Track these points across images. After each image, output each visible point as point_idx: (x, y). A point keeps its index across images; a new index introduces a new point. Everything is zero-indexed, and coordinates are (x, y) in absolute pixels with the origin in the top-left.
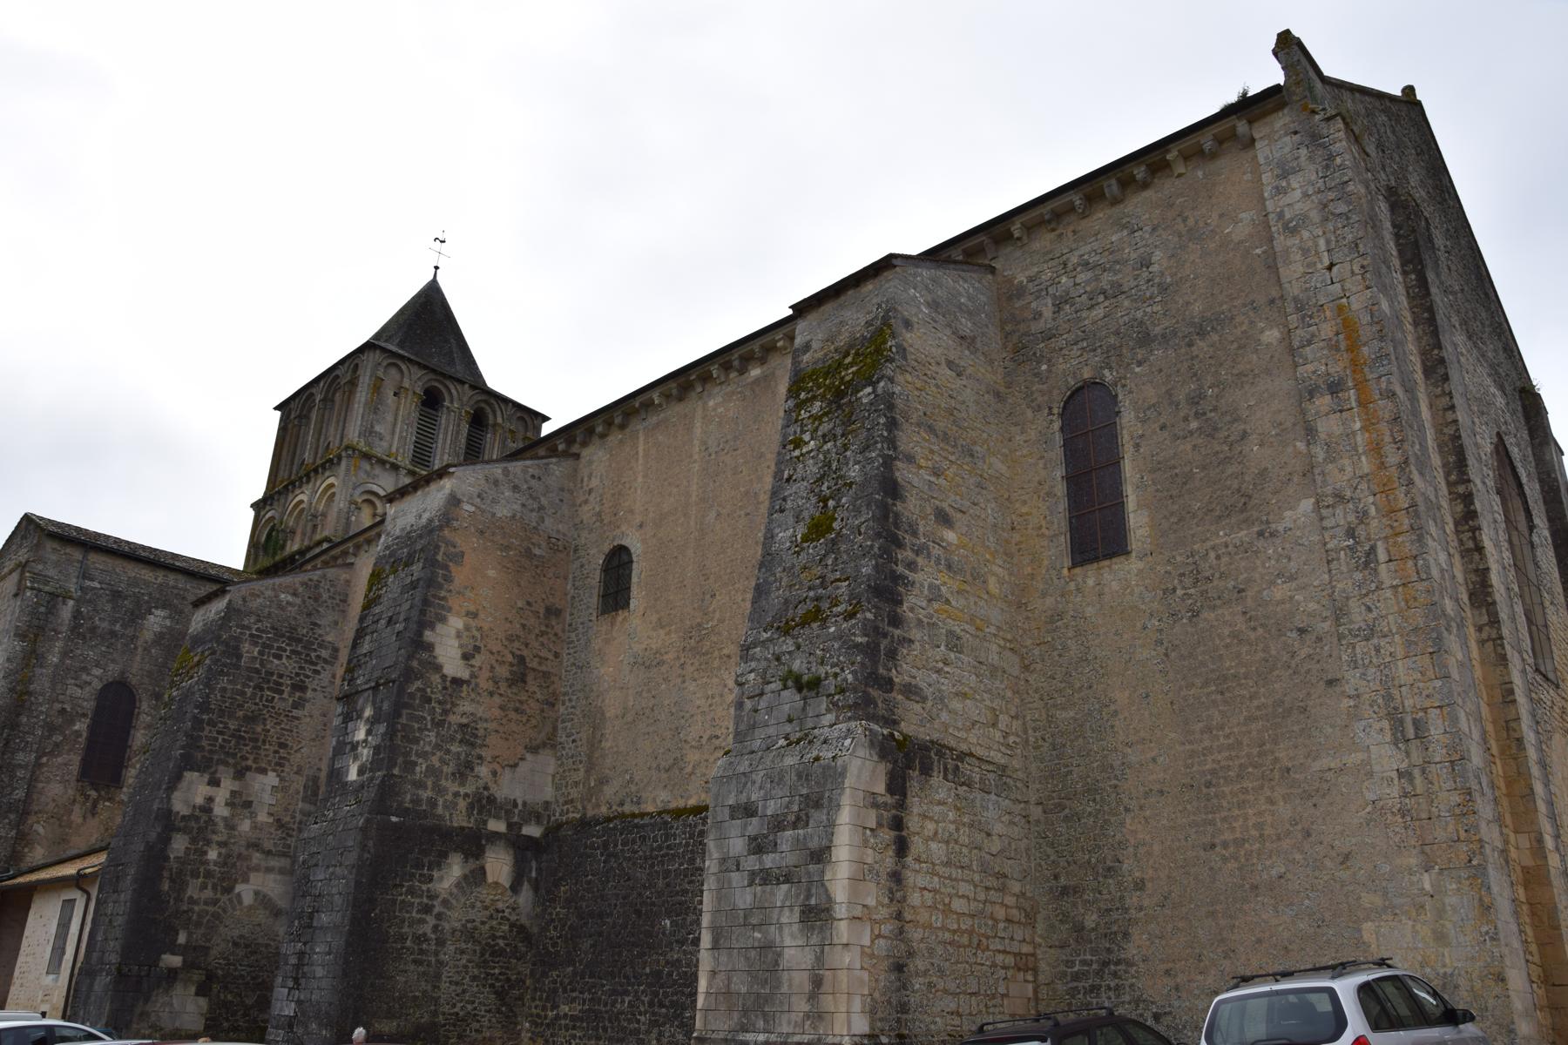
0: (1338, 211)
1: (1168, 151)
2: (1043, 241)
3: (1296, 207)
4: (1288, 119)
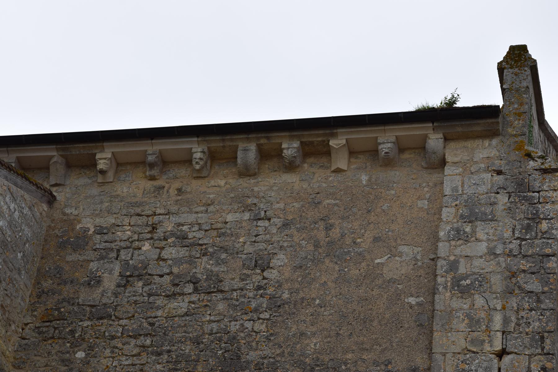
0: (528, 287)
1: (334, 135)
2: (133, 187)
3: (477, 263)
4: (494, 153)
